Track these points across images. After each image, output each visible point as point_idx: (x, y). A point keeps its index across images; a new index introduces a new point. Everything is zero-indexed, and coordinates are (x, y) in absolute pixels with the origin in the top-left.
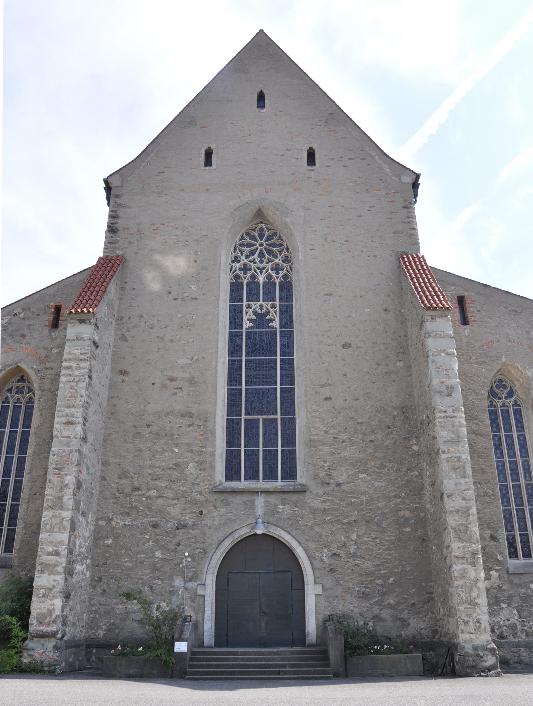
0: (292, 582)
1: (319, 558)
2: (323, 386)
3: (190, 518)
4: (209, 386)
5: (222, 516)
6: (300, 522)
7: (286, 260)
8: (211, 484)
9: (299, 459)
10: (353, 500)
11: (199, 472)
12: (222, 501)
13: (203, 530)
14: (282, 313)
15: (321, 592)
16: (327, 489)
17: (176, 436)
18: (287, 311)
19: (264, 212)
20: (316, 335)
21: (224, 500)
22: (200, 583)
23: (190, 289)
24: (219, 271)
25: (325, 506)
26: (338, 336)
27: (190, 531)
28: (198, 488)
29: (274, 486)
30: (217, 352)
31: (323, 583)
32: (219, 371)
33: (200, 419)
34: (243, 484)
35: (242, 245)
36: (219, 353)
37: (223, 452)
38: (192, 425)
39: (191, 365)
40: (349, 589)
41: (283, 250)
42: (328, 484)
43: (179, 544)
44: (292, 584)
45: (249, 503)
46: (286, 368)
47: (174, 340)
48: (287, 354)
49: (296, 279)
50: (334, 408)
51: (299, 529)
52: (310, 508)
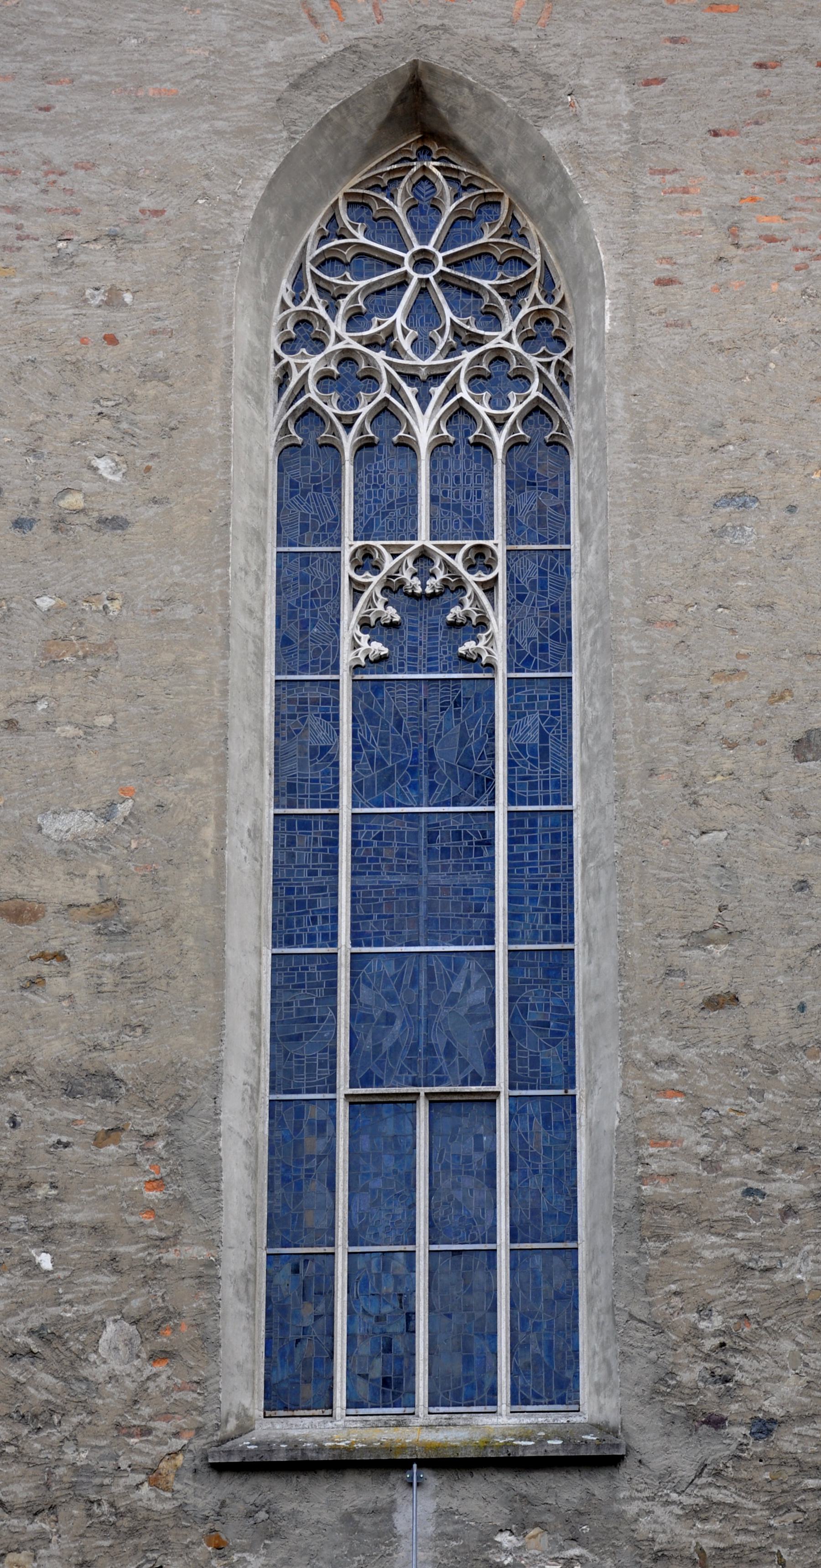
2: (699, 939)
4: (190, 942)
7: (545, 332)
8: (199, 1430)
9: (591, 1298)
11: (150, 1369)
12: (250, 1515)
14: (517, 596)
16: (716, 1449)
17: (43, 1191)
18: (543, 585)
19: (439, 97)
20: (675, 696)
21: (258, 1507)
23: (88, 475)
24: (225, 388)
26: (777, 697)
28: (144, 1451)
29: (478, 1437)
30: (222, 779)
32: (233, 873)
34: (340, 1427)
35: (327, 262)
36: (231, 784)
37: (253, 1269)
38: (112, 1133)
39: (103, 840)
41: (525, 288)
42: (717, 1422)
45: (367, 1523)
46: (533, 856)
47: (22, 724)
48: (539, 792)
49: (588, 426)
50: (748, 1045)
52: (636, 1544)
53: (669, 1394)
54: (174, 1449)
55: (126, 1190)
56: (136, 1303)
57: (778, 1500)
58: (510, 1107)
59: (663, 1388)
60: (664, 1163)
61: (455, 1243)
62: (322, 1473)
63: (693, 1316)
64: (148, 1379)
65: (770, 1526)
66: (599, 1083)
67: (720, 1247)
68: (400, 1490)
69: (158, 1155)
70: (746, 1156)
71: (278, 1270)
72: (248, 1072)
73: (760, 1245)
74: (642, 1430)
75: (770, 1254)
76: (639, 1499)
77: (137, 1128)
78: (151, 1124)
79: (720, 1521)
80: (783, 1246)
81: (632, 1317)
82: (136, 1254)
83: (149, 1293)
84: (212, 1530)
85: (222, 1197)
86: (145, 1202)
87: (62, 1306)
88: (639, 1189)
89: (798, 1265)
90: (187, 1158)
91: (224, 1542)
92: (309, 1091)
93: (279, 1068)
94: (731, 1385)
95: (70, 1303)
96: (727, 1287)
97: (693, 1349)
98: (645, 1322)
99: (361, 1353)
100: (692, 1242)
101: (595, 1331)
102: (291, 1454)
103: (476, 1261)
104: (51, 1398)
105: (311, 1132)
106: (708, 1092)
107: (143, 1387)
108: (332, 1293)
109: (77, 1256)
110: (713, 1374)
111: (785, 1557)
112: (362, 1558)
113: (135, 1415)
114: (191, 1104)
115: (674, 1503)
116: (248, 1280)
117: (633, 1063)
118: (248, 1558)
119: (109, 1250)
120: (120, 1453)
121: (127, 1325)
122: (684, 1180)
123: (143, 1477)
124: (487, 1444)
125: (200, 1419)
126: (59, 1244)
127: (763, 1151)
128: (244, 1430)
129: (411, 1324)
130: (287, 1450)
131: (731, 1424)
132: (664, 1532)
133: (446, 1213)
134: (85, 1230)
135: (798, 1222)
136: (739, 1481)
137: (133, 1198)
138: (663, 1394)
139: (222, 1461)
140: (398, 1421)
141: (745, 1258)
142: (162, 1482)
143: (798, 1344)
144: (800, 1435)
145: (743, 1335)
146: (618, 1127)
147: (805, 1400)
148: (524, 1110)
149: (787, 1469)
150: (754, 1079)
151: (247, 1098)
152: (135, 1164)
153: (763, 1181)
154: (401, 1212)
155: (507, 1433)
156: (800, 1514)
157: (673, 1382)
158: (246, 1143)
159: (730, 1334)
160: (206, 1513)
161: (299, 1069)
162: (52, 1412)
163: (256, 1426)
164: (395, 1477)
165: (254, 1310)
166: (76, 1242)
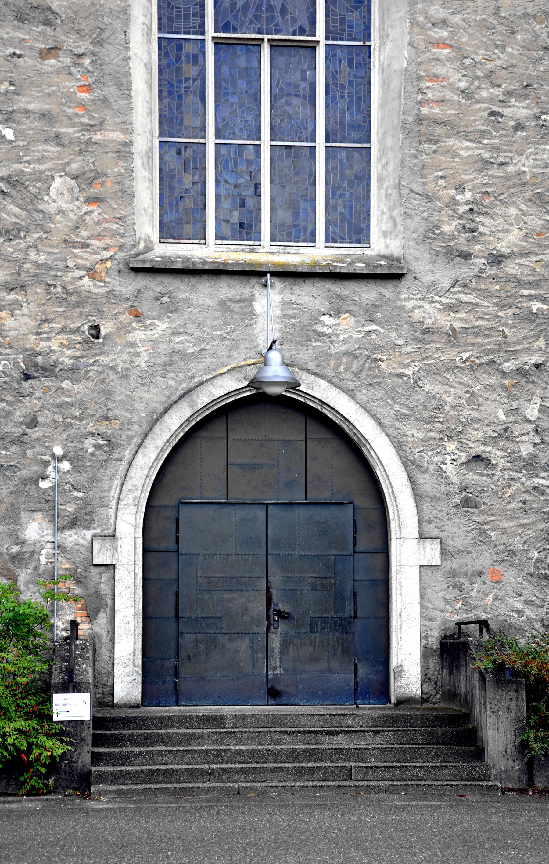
0: (355, 532)
1: (432, 468)
3: (62, 345)
5: (158, 341)
6: (383, 365)
8: (121, 247)
9: (380, 179)
10: (536, 306)
11: (86, 208)
12: (157, 299)
13: (103, 381)
15: (437, 561)
16: (465, 272)
21: (163, 295)
22: (98, 531)
25: (455, 320)
27: (66, 384)
29: (308, 260)
31: (442, 534)
33: (78, 32)
34: (211, 251)
37: (151, 149)
38: (52, 51)
40: (512, 553)
42: (466, 256)
43: (33, 423)
44: (355, 538)
45: (236, 307)
51: (379, 384)
52: (412, 324)
53: (435, 238)
54: (105, 257)
55: (64, 91)
56: (75, 166)
57: (504, 302)
58: (326, 52)
59: (431, 235)
60: (436, 93)
61: (288, 141)
62: (205, 277)
63: (453, 192)
64: (85, 214)
65: (498, 316)
66: (390, 37)
67: (472, 149)
68: (258, 289)
69: (86, 69)
70: (491, 90)
71: (167, 152)
72: (145, 16)
73: (498, 148)
74: (417, 259)
75: (505, 154)
76: (414, 299)
77: (70, 49)
78: (80, 47)
79: (466, 313)
80: (514, 149)
81: (412, 191)
82: (74, 134)
83: (84, 160)
84: (132, 306)
85: (133, 101)
86: (78, 100)
87: (23, 164)
88: (419, 110)
89: (523, 162)
90: (107, 72)
91: (140, 313)
92: (185, 33)
93: (164, 15)
94: (476, 234)
95: (29, 163)
96: (475, 175)
97: (452, 212)
98: (420, 195)
99: (224, 206)
100: (453, 145)
101: (384, 199)
102: (185, 264)
103: (302, 153)
104: (18, 221)
105: (188, 62)
106: (467, 45)
107: (82, 218)
108: (204, 168)
109: (31, 132)
110: (464, 227)
111: (507, 333)
112: (233, 326)
113: (77, 236)
114: (108, 35)
115: (436, 302)
116: (149, 157)
117: (417, 24)
118: (157, 323)
119: (54, 130)
120: (68, 258)
121: (69, 179)
122: (449, 105)
123: (84, 273)
124: (315, 264)
125: (122, 240)
126: (18, 123)
127: (503, 86)
128: (148, 249)
129: (258, 190)
130: (183, 262)
131: (475, 257)
132: (430, 318)
133: (282, 121)
134: (36, 115)
135: (524, 134)
136: (480, 290)
137: (70, 98)
138: (431, 238)
139: (139, 266)
140: (251, 249)
141: (488, 156)
142: (97, 276)
143: (521, 210)
144: (519, 264)
145: (485, 204)
146: (406, 68)
147: (524, 244)
148: (335, 55)
149: (510, 284)
150: (499, 38)
151: (145, 34)
152: (70, 74)
153: (502, 107)
154: (251, 119)
155: (326, 258)
156: (518, 310)
157: (439, 232)
158: (145, 65)
159: (477, 204)
160: (128, 296)
161: (178, 17)
162: (19, 230)
163: (155, 247)
164: (254, 281)
165: (152, 176)
166: (30, 123)
